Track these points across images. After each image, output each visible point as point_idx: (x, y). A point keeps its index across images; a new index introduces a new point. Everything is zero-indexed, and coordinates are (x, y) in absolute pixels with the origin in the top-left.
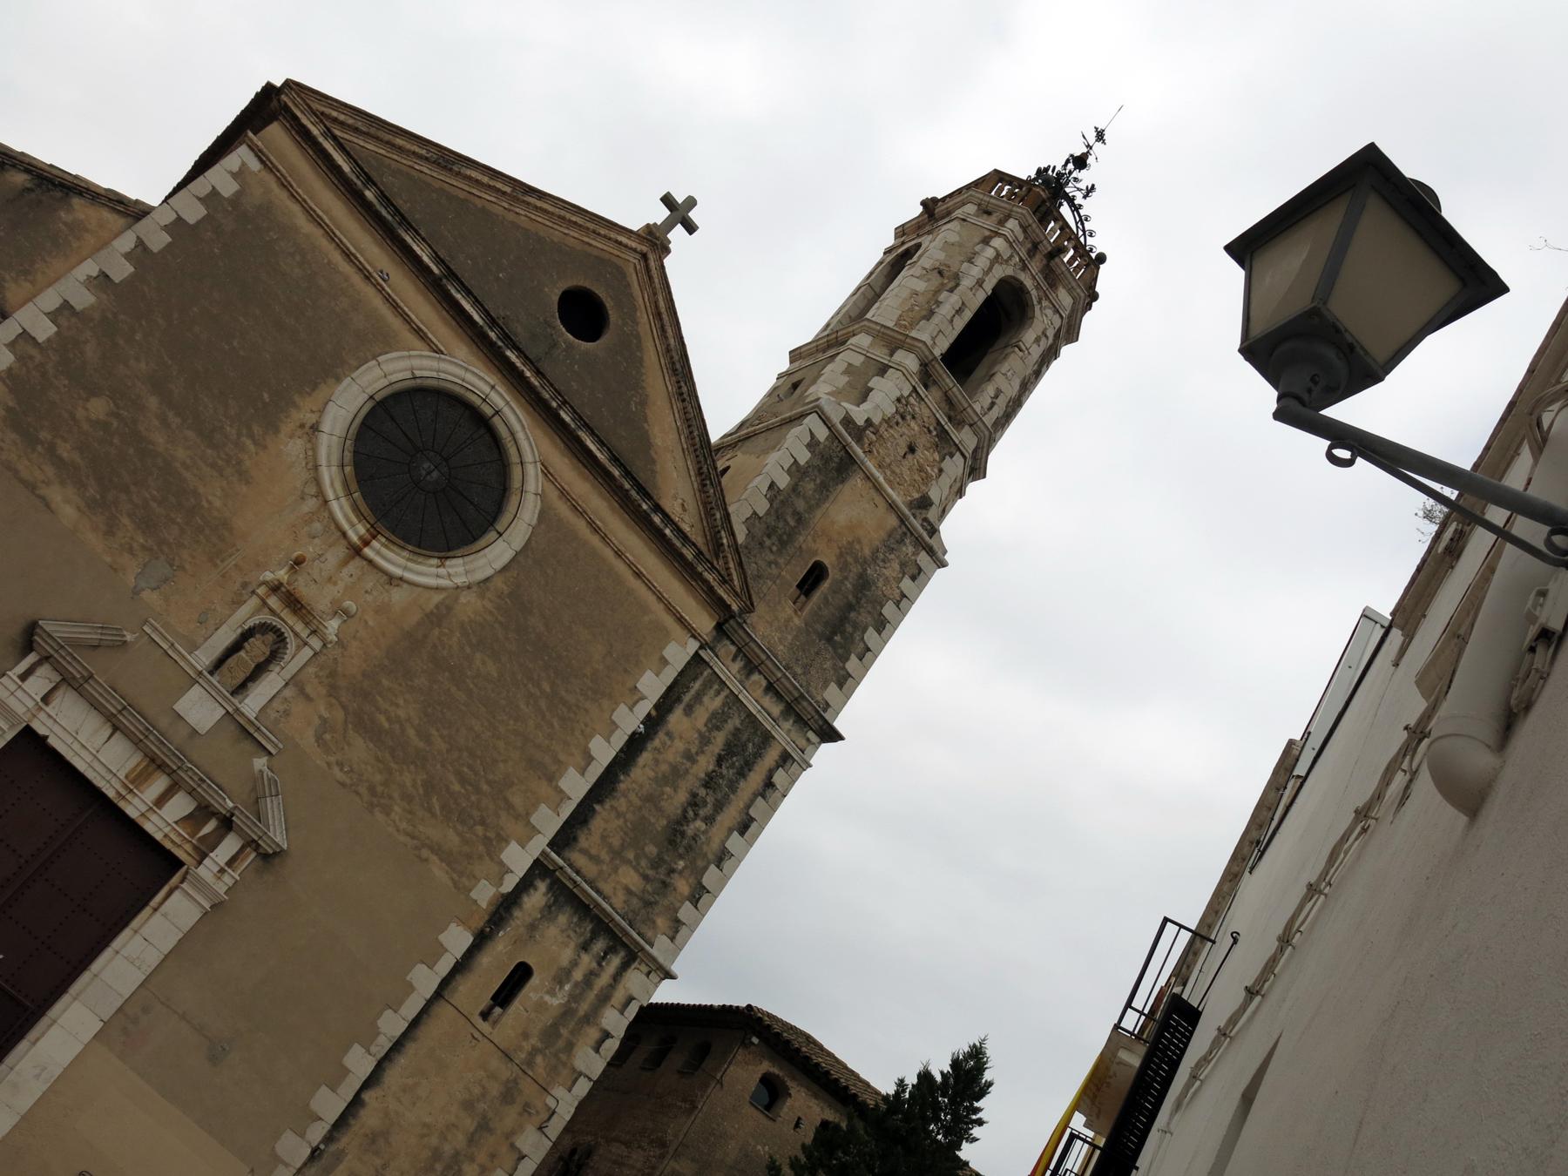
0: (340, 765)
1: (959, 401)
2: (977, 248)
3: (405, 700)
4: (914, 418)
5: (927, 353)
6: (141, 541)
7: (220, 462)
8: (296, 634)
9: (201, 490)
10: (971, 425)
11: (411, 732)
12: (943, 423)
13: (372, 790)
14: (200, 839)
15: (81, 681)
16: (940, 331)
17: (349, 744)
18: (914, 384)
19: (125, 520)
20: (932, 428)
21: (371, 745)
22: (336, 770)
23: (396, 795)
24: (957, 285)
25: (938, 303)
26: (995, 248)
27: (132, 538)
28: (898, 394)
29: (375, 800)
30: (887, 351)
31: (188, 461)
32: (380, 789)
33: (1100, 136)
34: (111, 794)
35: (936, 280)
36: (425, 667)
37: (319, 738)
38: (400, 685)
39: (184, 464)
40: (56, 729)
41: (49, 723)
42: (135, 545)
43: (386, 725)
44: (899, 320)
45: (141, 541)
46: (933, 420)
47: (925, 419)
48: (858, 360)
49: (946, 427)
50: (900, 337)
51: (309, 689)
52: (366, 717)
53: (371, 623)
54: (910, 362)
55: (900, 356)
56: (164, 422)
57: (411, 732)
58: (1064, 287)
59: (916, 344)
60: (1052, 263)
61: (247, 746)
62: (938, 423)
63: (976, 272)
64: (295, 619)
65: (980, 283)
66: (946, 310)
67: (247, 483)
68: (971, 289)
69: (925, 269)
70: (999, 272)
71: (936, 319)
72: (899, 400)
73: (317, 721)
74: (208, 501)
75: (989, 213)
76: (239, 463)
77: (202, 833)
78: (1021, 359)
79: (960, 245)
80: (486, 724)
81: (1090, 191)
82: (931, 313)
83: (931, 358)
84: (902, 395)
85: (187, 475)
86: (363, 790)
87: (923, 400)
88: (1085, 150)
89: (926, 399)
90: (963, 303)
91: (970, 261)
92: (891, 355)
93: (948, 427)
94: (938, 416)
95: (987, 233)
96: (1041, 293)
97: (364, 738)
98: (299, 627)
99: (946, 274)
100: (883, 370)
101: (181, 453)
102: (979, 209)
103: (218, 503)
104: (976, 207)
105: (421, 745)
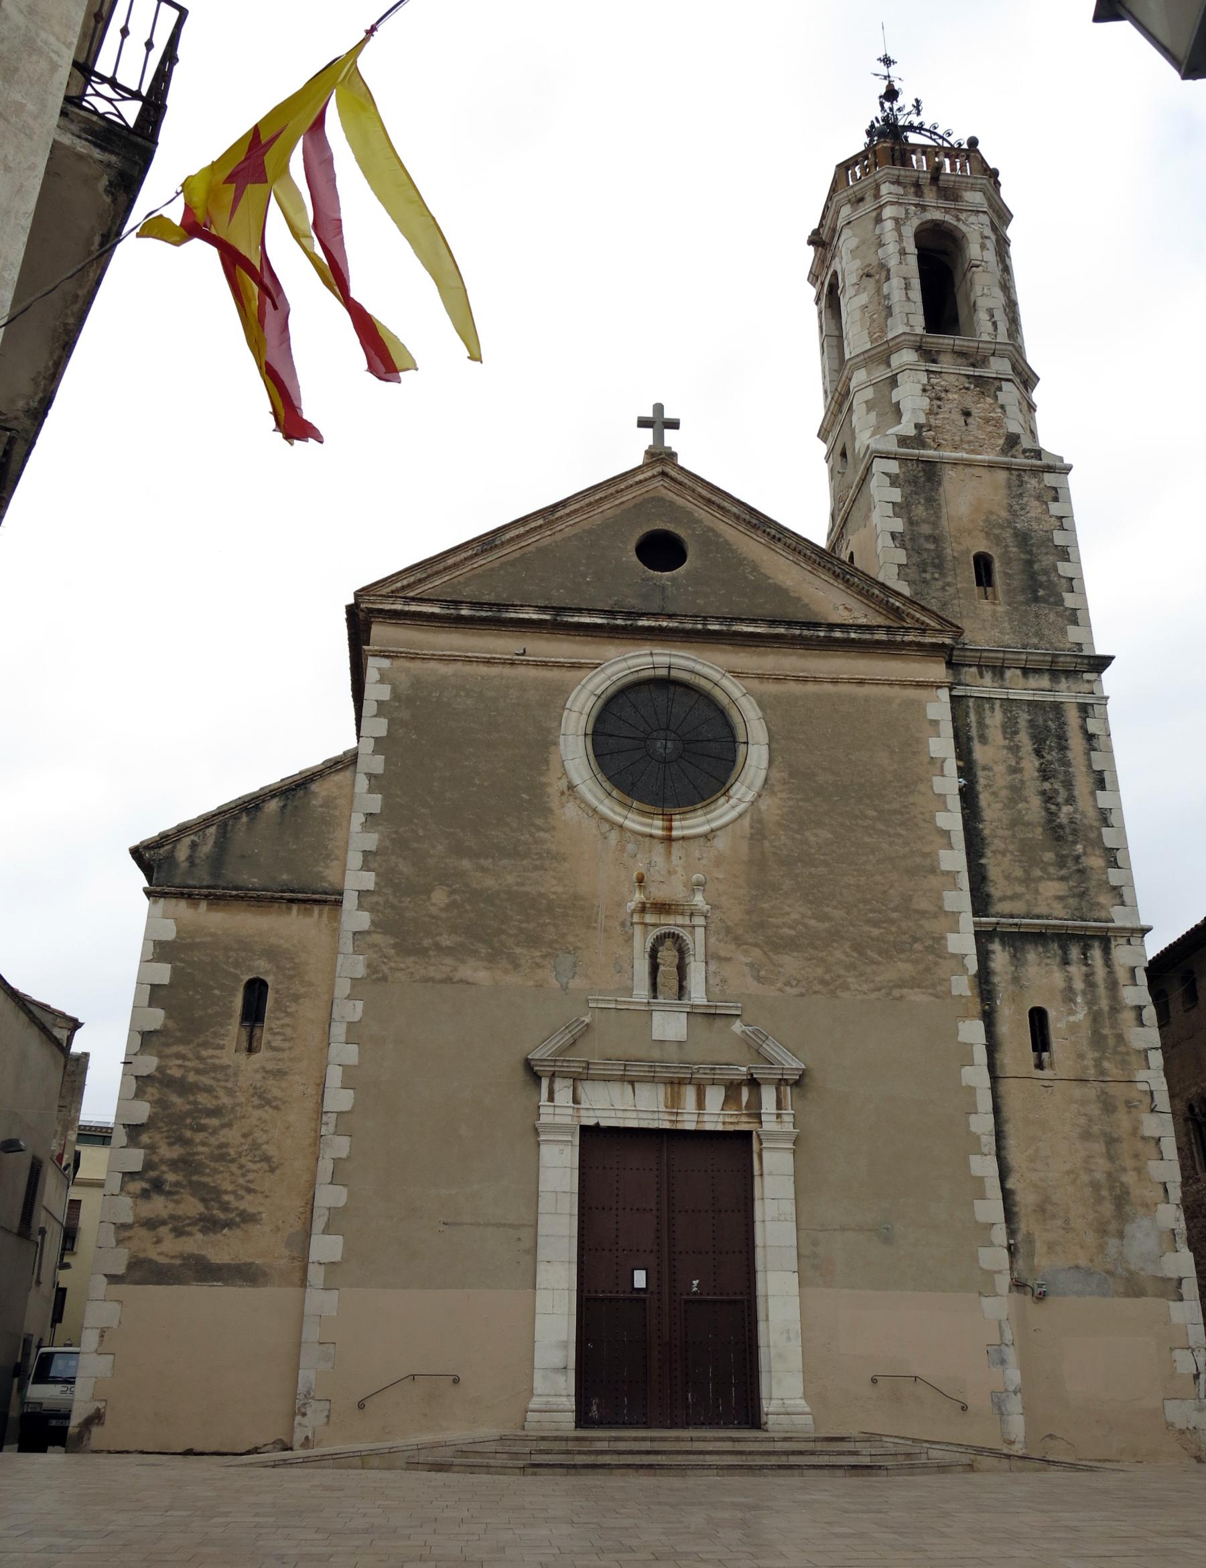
0: (788, 984)
1: (968, 347)
2: (877, 232)
3: (789, 906)
4: (947, 391)
5: (913, 338)
6: (539, 954)
7: (537, 863)
8: (682, 926)
9: (543, 890)
10: (993, 355)
11: (812, 922)
12: (972, 373)
13: (823, 982)
14: (747, 1107)
15: (585, 1071)
16: (907, 314)
17: (781, 966)
18: (923, 368)
19: (518, 950)
20: (967, 385)
21: (796, 954)
22: (788, 989)
23: (842, 972)
24: (888, 271)
25: (887, 297)
26: (890, 218)
27: (533, 958)
28: (920, 387)
29: (832, 987)
30: (882, 367)
31: (519, 880)
32: (827, 977)
33: (887, 61)
34: (667, 1125)
35: (870, 284)
36: (781, 873)
37: (758, 979)
38: (776, 899)
39: (518, 884)
40: (598, 1113)
41: (591, 1113)
42: (537, 960)
43: (792, 932)
44: (870, 337)
45: (539, 954)
46: (963, 379)
47: (956, 384)
48: (869, 393)
49: (976, 374)
50: (882, 348)
51: (723, 954)
52: (774, 939)
53: (721, 876)
54: (907, 356)
55: (896, 360)
56: (484, 870)
57: (812, 922)
58: (966, 190)
59: (898, 340)
60: (941, 184)
61: (719, 1023)
62: (968, 376)
63: (892, 248)
64: (672, 917)
65: (903, 252)
66: (897, 295)
67: (564, 860)
68: (901, 263)
69: (854, 284)
70: (909, 231)
71: (896, 310)
72: (924, 390)
73: (747, 969)
74: (553, 893)
75: (861, 200)
76: (548, 852)
77: (744, 1104)
78: (984, 271)
79: (863, 242)
80: (855, 873)
81: (917, 106)
82: (889, 309)
83: (918, 338)
84: (924, 385)
85: (527, 889)
86: (818, 987)
87: (941, 372)
88: (886, 83)
89: (944, 370)
90: (905, 279)
91: (881, 245)
92: (889, 366)
93: (978, 372)
94: (962, 372)
95: (874, 214)
96: (955, 212)
97: (786, 954)
98: (680, 920)
99: (873, 272)
100: (893, 382)
101: (510, 879)
102: (852, 205)
103: (560, 889)
104: (849, 206)
105: (827, 925)
